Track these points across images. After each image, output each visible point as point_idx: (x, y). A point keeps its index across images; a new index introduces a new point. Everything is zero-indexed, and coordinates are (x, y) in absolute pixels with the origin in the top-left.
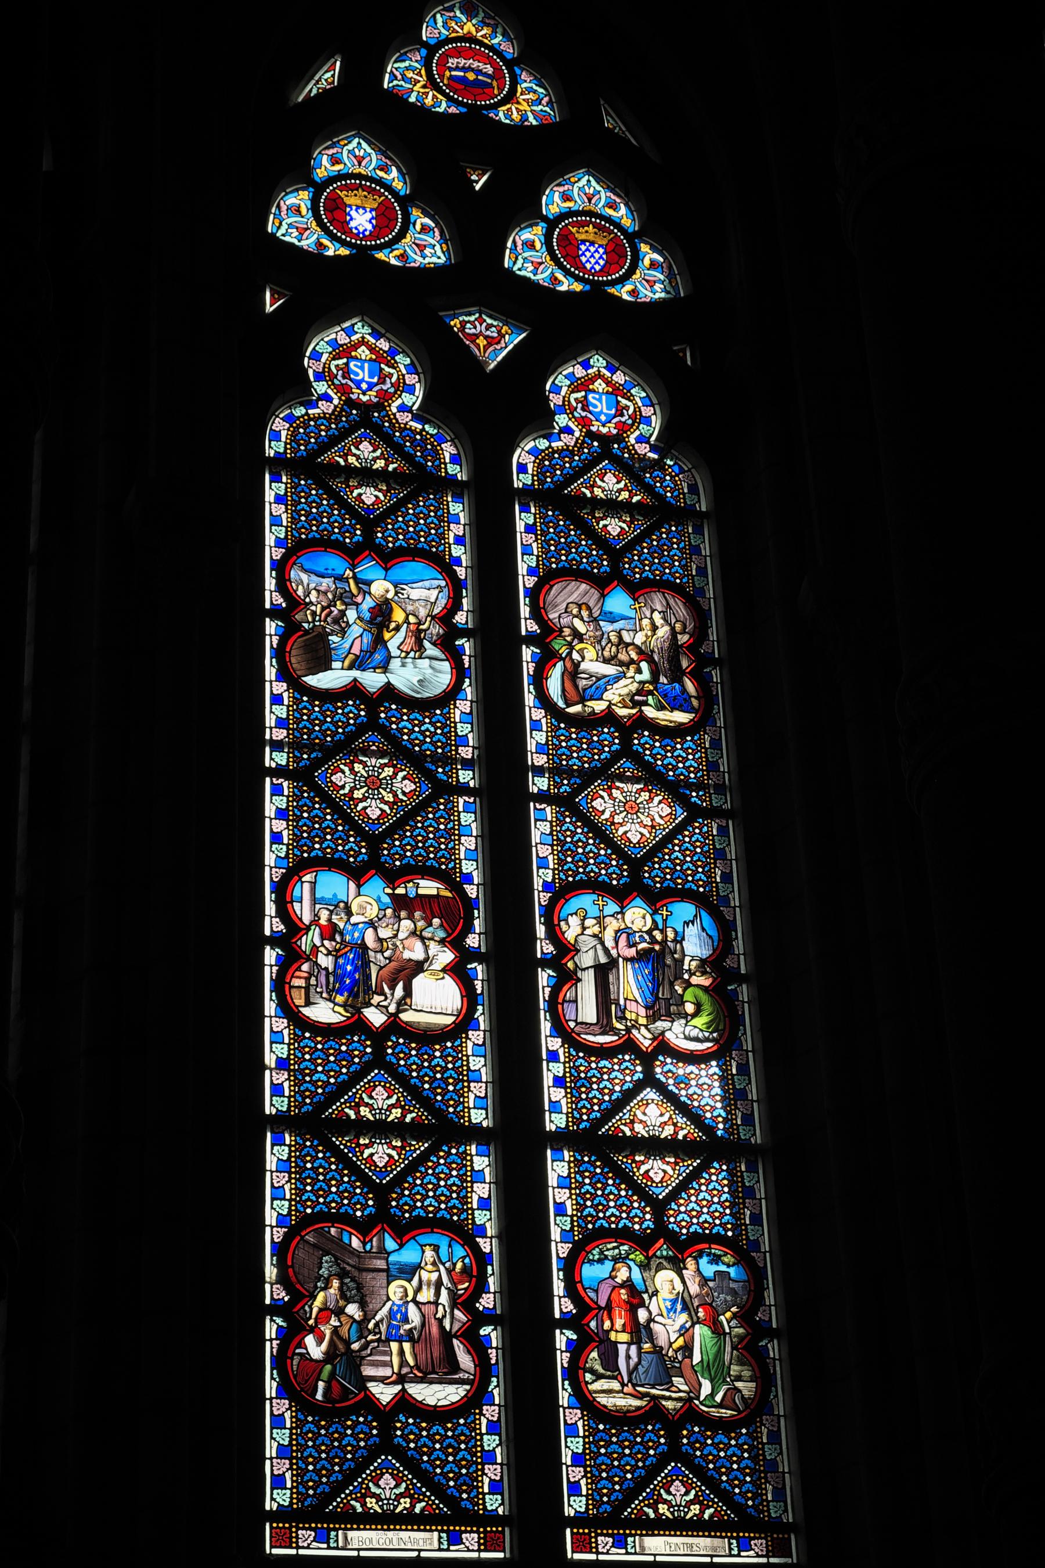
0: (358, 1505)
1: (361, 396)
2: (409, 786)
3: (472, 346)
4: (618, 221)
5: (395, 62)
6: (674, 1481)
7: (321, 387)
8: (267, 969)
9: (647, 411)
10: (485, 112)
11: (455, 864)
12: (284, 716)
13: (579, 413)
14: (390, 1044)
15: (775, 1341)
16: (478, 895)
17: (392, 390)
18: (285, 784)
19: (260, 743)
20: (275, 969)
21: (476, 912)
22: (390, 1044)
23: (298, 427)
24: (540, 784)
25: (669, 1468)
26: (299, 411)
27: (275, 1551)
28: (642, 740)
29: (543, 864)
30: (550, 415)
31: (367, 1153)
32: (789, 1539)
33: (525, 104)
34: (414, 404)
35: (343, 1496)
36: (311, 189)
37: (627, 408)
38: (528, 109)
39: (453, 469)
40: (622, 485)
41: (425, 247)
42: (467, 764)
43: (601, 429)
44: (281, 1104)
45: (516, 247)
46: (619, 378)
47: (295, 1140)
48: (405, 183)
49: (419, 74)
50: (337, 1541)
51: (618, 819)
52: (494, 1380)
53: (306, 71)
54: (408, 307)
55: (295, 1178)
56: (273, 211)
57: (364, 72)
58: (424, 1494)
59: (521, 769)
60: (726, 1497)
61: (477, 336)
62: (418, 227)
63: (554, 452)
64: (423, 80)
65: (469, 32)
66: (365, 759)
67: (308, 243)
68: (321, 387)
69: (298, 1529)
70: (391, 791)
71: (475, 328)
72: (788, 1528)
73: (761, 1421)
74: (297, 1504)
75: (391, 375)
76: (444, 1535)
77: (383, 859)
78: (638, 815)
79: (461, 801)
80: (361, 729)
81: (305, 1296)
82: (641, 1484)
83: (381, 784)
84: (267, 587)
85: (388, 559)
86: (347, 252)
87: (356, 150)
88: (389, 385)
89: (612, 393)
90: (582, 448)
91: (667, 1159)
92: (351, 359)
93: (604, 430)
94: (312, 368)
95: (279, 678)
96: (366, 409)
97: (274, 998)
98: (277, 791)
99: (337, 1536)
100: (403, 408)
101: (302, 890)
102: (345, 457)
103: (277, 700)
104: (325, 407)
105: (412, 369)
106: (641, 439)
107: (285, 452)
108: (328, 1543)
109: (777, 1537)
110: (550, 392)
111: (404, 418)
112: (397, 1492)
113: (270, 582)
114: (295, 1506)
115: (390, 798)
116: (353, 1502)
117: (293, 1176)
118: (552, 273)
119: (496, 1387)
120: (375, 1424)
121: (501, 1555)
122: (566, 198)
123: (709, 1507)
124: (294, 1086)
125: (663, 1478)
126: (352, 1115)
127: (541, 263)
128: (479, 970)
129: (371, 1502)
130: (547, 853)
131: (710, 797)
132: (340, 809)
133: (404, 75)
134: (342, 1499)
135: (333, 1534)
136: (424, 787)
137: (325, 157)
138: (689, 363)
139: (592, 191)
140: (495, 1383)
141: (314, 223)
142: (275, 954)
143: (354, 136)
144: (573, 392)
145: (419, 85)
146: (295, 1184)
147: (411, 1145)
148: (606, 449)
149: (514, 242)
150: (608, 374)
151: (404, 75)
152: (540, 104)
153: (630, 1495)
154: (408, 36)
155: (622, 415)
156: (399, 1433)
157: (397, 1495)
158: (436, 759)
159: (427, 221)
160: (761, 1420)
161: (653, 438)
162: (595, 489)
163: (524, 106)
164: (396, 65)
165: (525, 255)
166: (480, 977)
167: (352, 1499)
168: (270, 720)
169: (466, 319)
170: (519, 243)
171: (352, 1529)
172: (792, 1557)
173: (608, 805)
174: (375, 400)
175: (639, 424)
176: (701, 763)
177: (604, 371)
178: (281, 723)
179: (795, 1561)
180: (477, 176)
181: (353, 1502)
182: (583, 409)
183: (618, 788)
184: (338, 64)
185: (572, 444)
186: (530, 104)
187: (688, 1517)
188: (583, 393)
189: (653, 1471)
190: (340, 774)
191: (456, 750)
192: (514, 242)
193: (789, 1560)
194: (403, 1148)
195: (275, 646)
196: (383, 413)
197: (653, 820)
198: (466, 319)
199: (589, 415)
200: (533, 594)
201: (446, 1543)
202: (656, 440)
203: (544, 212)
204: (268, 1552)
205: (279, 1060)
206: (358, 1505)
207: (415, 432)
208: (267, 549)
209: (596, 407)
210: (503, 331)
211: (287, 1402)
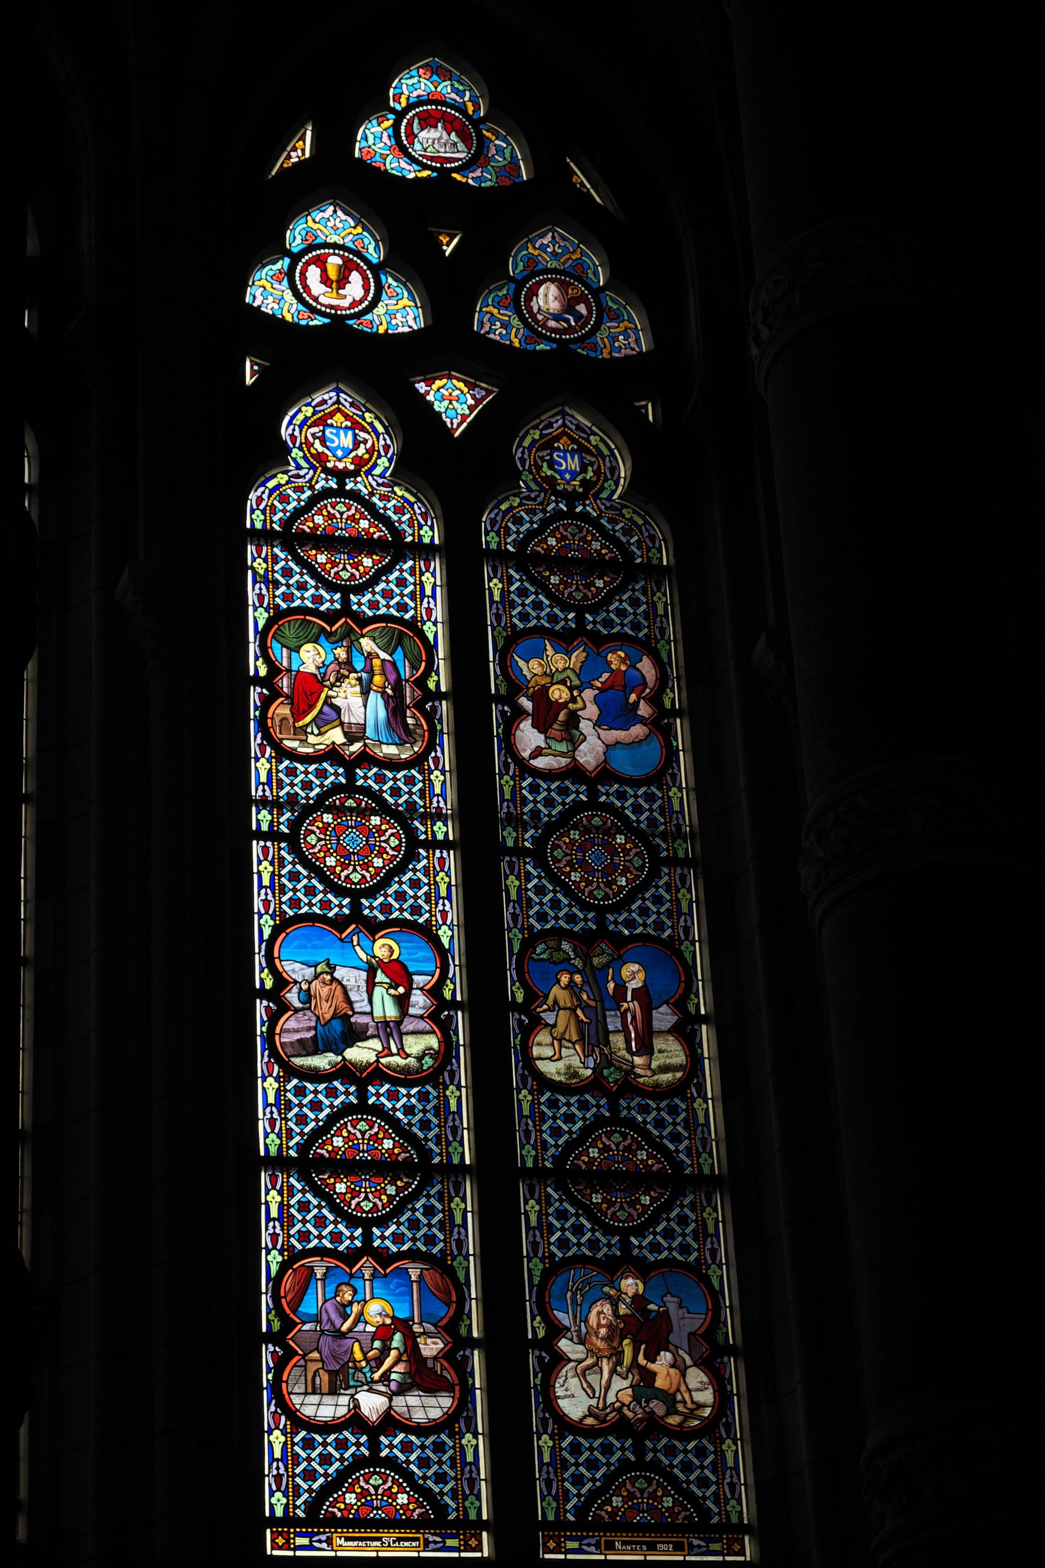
1: (337, 464)
13: (317, 444)
19: (247, 801)
27: (547, 1556)
41: (400, 313)
43: (337, 464)
54: (380, 370)
57: (337, 140)
75: (365, 442)
81: (701, 1336)
89: (350, 428)
92: (334, 432)
133: (373, 139)
138: (651, 418)
143: (550, 230)
151: (373, 139)
154: (375, 103)
179: (748, 1559)
184: (309, 134)
193: (742, 1559)
204: (269, 1553)
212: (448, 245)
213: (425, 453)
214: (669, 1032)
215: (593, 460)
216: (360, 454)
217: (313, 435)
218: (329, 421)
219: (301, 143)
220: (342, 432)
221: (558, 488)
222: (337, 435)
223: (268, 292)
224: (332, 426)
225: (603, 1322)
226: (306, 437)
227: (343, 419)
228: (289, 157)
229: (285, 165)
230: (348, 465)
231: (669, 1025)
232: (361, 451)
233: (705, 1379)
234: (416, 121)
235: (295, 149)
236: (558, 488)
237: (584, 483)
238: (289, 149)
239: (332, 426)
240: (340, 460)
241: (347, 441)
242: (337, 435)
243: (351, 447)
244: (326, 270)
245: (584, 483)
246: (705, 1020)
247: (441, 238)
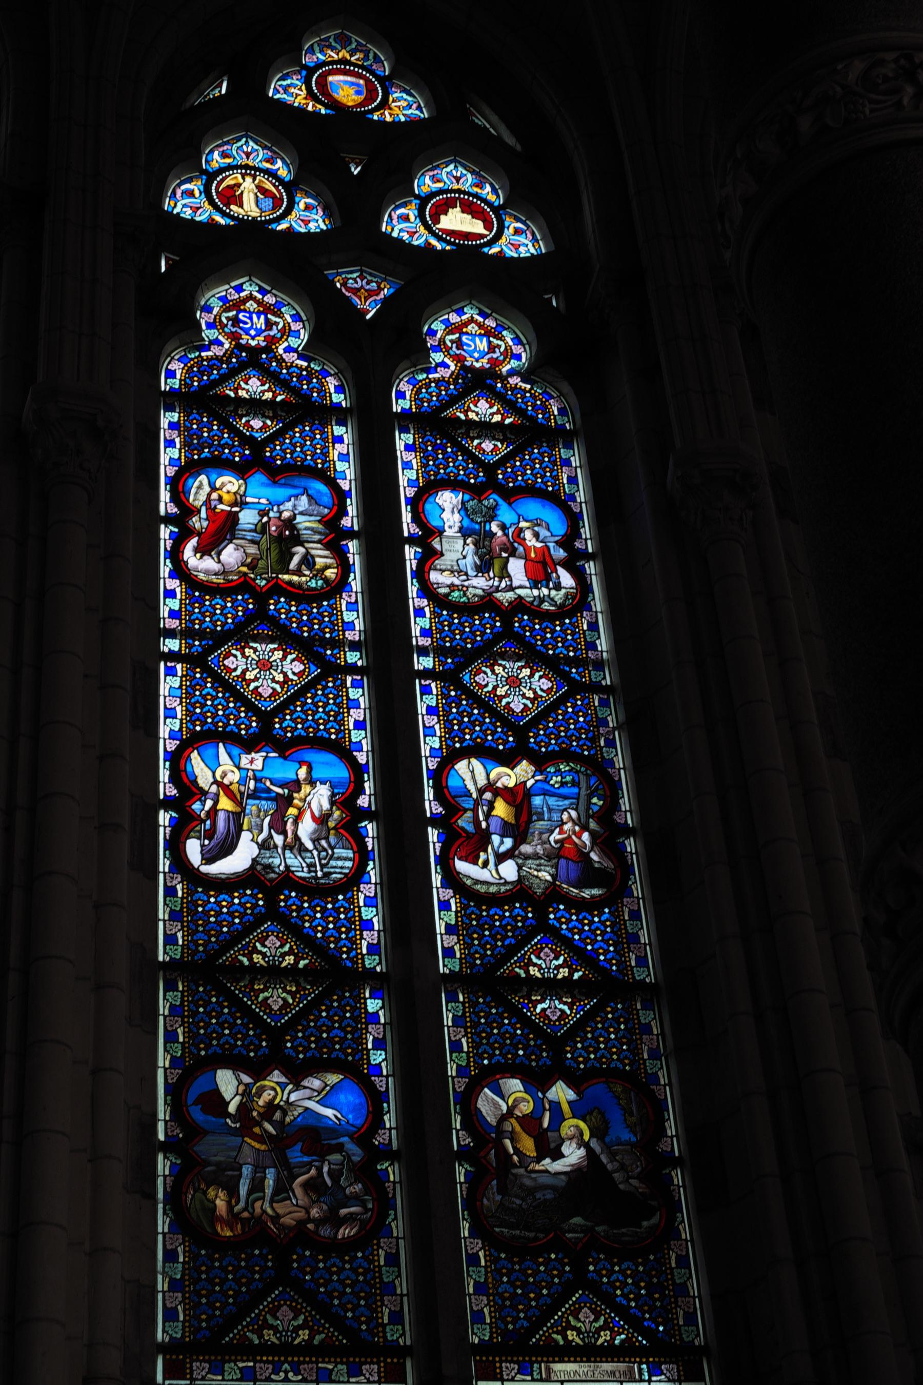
0: (559, 1338)
2: (298, 667)
3: (354, 297)
4: (484, 196)
5: (278, 80)
6: (282, 1306)
7: (212, 334)
8: (161, 829)
9: (295, 326)
10: (370, 116)
11: (597, 751)
12: (427, 627)
14: (282, 897)
15: (396, 1166)
16: (368, 761)
17: (502, 358)
18: (433, 685)
20: (168, 830)
21: (366, 776)
22: (282, 897)
23: (192, 366)
24: (425, 663)
25: (577, 1295)
26: (421, 377)
28: (278, 606)
29: (170, 714)
30: (425, 352)
31: (261, 997)
33: (397, 109)
34: (299, 346)
35: (545, 1329)
36: (204, 177)
37: (499, 347)
38: (399, 112)
39: (337, 398)
40: (495, 409)
42: (354, 646)
43: (475, 364)
44: (454, 965)
45: (392, 220)
46: (270, 299)
47: (468, 997)
48: (289, 171)
49: (300, 89)
50: (541, 1372)
51: (250, 675)
52: (392, 1212)
55: (471, 1033)
56: (385, 219)
58: (623, 1327)
59: (407, 649)
60: (338, 1322)
61: (358, 290)
62: (511, 230)
63: (431, 382)
64: (304, 93)
65: (343, 57)
66: (503, 663)
67: (201, 217)
68: (212, 334)
69: (501, 1362)
70: (282, 672)
71: (357, 282)
73: (378, 1244)
74: (189, 1337)
76: (644, 1366)
77: (275, 732)
78: (518, 688)
79: (349, 679)
80: (497, 637)
82: (244, 1309)
83: (521, 683)
84: (404, 519)
85: (511, 495)
86: (232, 223)
87: (454, 172)
88: (499, 354)
89: (484, 335)
90: (230, 357)
91: (564, 999)
92: (242, 313)
93: (478, 365)
94: (204, 319)
95: (172, 576)
96: (254, 352)
97: (439, 870)
98: (171, 672)
99: (540, 1368)
100: (289, 349)
102: (466, 413)
103: (419, 612)
104: (442, 373)
105: (296, 318)
106: (289, 349)
107: (411, 408)
108: (532, 1375)
109: (687, 1361)
110: (426, 335)
111: (291, 357)
112: (296, 1324)
113: (406, 516)
114: (495, 1340)
115: (280, 678)
116: (554, 1336)
117: (469, 1030)
118: (426, 240)
119: (393, 1220)
120: (566, 1260)
122: (224, 155)
123: (319, 1333)
124: (464, 949)
125: (269, 1303)
126: (245, 961)
127: (198, 208)
128: (370, 828)
129: (268, 1335)
130: (434, 722)
131: (589, 673)
132: (486, 704)
133: (290, 90)
134: (544, 1332)
135: (536, 1366)
136: (215, 661)
137: (427, 177)
139: (249, 150)
140: (392, 1217)
141: (422, 228)
142: (169, 816)
144: (448, 334)
145: (299, 98)
146: (471, 1038)
147: (305, 989)
148: (477, 381)
149: (390, 216)
150: (259, 296)
152: (410, 108)
153: (232, 1321)
155: (494, 352)
156: (295, 1265)
157: (295, 1327)
158: (576, 662)
159: (309, 201)
160: (379, 1243)
161: (300, 349)
162: (470, 413)
163: (396, 111)
164: (279, 83)
165: (184, 202)
166: (370, 835)
167: (554, 1332)
168: (416, 631)
169: (349, 276)
170: (395, 216)
171: (554, 1362)
173: (289, 667)
174: (263, 344)
175: (288, 336)
176: (580, 643)
177: (255, 294)
178: (425, 633)
180: (351, 163)
181: (554, 1336)
182: (458, 348)
183: (500, 665)
185: (448, 375)
186: (404, 106)
187: (296, 1342)
188: (457, 335)
189: (258, 1297)
190: (482, 674)
191: (344, 635)
192: (390, 216)
194: (297, 992)
195: (414, 569)
196: (272, 355)
197: (535, 692)
198: (349, 276)
199: (463, 353)
200: (416, 503)
201: (646, 1374)
202: (303, 349)
203: (417, 192)
205: (448, 926)
206: (559, 1338)
207: (301, 369)
208: (162, 467)
209: (470, 346)
210: (382, 286)
211: (180, 1236)
212: (605, 678)
213: (335, 329)
214: (205, 1133)
217: (227, 318)
218: (464, 330)
220: (477, 339)
222: (474, 341)
223: (187, 202)
224: (467, 333)
227: (477, 328)
231: (209, 1138)
233: (574, 585)
234: (462, 866)
239: (467, 333)
240: (477, 361)
241: (483, 345)
242: (474, 341)
243: (486, 350)
244: (242, 181)
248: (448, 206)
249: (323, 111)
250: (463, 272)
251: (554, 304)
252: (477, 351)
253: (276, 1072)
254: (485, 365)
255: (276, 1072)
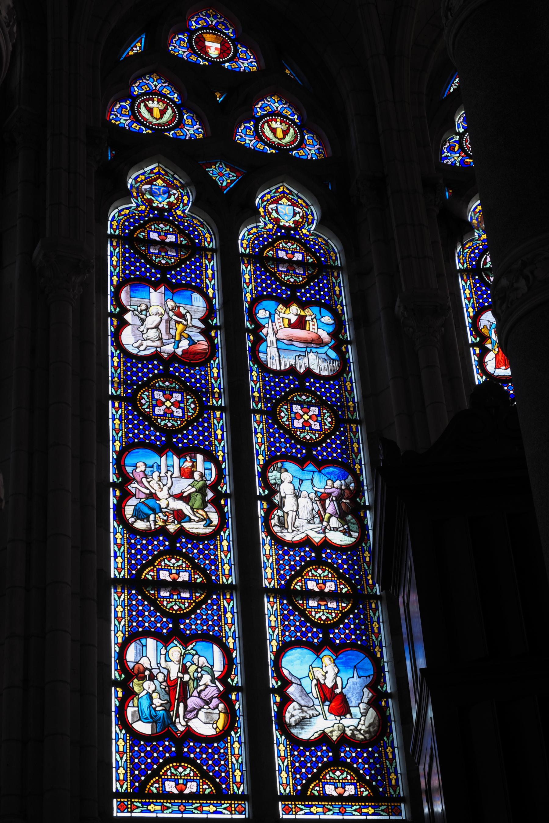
32: (400, 806)
42: (256, 411)
43: (159, 205)
53: (129, 44)
72: (400, 800)
75: (299, 213)
92: (152, 187)
93: (287, 225)
101: (129, 460)
121: (243, 816)
133: (179, 47)
172: (402, 816)
180: (218, 99)
186: (247, 63)
199: (279, 217)
213: (208, 198)
215: (300, 210)
216: (171, 201)
219: (139, 43)
221: (153, 204)
224: (155, 185)
225: (280, 639)
226: (268, 210)
228: (132, 50)
229: (130, 54)
230: (165, 205)
232: (297, 218)
235: (135, 46)
236: (192, 27)
237: (295, 222)
238: (132, 46)
245: (295, 222)
246: (369, 508)
247: (216, 94)
248: (276, 128)
249: (274, 152)
250: (277, 166)
251: (330, 188)
252: (286, 214)
253: (212, 495)
254: (291, 224)
255: (212, 495)
